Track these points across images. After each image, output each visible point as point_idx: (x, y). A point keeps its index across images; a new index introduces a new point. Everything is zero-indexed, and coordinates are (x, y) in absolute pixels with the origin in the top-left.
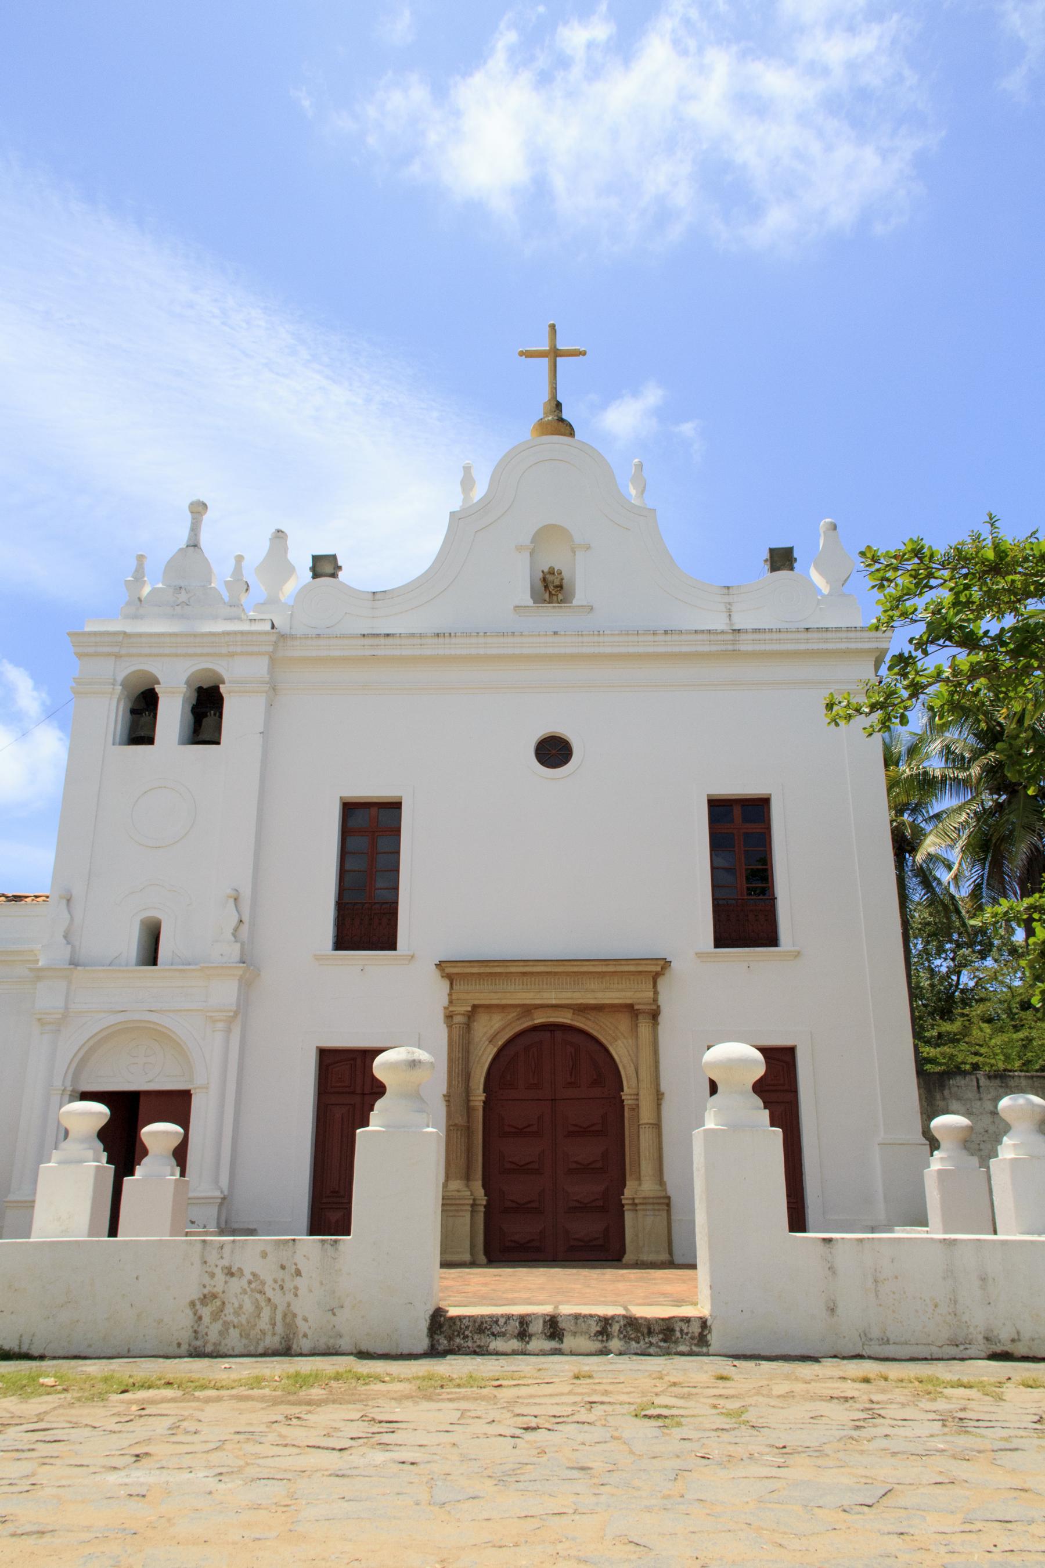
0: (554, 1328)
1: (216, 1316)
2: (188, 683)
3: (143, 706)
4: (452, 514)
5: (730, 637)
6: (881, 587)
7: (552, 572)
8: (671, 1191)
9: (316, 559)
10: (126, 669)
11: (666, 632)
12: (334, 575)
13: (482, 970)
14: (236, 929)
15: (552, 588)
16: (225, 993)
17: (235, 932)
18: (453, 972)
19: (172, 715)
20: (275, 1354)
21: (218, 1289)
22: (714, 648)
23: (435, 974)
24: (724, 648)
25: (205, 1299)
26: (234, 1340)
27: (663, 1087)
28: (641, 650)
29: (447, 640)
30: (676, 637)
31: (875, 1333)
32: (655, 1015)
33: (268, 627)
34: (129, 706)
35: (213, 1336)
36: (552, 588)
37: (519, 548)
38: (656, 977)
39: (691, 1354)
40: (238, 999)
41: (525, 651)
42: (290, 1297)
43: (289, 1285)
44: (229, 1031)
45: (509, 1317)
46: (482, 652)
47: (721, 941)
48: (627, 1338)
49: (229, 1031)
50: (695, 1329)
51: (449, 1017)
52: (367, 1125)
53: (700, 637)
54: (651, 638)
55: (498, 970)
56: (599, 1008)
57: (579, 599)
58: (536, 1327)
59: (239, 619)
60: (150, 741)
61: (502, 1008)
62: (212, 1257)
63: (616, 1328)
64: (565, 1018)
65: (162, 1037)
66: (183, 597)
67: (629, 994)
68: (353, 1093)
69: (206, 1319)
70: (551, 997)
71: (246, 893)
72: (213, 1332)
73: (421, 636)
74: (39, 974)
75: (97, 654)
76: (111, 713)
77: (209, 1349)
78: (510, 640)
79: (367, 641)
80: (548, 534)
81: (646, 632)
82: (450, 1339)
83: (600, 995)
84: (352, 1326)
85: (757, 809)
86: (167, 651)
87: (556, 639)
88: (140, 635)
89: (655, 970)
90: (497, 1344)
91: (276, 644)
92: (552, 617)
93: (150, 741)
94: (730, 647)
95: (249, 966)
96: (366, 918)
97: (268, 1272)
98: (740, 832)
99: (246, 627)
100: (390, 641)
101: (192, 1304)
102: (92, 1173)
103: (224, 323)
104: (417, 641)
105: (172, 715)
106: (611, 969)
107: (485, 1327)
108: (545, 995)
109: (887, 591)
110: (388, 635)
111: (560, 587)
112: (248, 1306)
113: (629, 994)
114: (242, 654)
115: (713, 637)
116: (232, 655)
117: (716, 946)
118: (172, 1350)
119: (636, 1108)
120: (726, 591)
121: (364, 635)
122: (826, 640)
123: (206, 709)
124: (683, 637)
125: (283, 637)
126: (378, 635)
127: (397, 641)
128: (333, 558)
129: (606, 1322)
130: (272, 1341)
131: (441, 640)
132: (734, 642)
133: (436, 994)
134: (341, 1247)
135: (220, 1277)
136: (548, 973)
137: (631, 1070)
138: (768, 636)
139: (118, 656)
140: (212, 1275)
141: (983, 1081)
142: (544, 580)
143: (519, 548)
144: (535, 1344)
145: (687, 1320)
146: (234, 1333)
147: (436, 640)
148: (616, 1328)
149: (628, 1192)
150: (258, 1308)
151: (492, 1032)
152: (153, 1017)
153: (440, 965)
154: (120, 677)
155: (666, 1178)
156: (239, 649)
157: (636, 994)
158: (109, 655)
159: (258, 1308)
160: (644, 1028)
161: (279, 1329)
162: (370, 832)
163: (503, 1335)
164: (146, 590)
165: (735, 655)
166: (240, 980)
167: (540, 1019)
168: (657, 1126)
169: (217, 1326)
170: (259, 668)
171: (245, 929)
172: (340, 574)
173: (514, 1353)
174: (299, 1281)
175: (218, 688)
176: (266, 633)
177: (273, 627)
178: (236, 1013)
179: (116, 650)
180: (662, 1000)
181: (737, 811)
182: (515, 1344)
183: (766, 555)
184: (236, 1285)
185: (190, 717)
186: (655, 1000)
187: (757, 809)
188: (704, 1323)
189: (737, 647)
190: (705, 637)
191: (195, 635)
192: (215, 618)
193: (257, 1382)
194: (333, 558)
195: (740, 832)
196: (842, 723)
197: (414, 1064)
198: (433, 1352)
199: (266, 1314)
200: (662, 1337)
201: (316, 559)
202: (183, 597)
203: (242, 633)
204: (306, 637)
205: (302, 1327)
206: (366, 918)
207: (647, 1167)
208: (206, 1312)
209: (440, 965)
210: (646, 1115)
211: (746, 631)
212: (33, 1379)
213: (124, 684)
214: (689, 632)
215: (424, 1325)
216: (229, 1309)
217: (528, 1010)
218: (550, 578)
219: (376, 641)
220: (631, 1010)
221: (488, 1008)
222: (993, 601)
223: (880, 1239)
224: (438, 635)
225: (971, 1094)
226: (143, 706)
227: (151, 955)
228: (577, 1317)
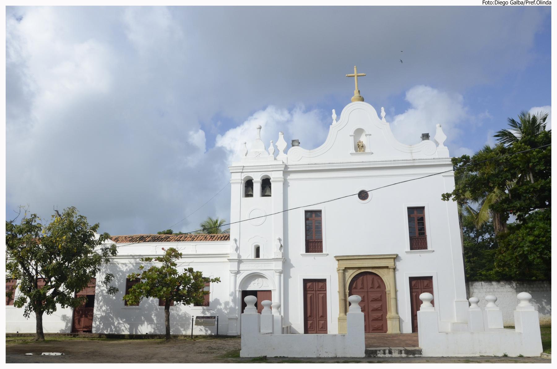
3: (249, 184)
10: (244, 176)
16: (279, 266)
18: (339, 259)
19: (257, 188)
33: (282, 163)
44: (280, 276)
49: (280, 276)
60: (251, 196)
71: (282, 238)
85: (318, 213)
89: (396, 258)
93: (251, 196)
96: (313, 244)
98: (416, 217)
105: (257, 188)
119: (389, 294)
123: (266, 184)
153: (335, 257)
157: (390, 263)
162: (313, 219)
170: (280, 175)
179: (241, 171)
183: (421, 135)
187: (318, 213)
195: (416, 217)
206: (313, 244)
210: (392, 295)
217: (360, 268)
218: (359, 144)
225: (479, 287)
227: (258, 255)
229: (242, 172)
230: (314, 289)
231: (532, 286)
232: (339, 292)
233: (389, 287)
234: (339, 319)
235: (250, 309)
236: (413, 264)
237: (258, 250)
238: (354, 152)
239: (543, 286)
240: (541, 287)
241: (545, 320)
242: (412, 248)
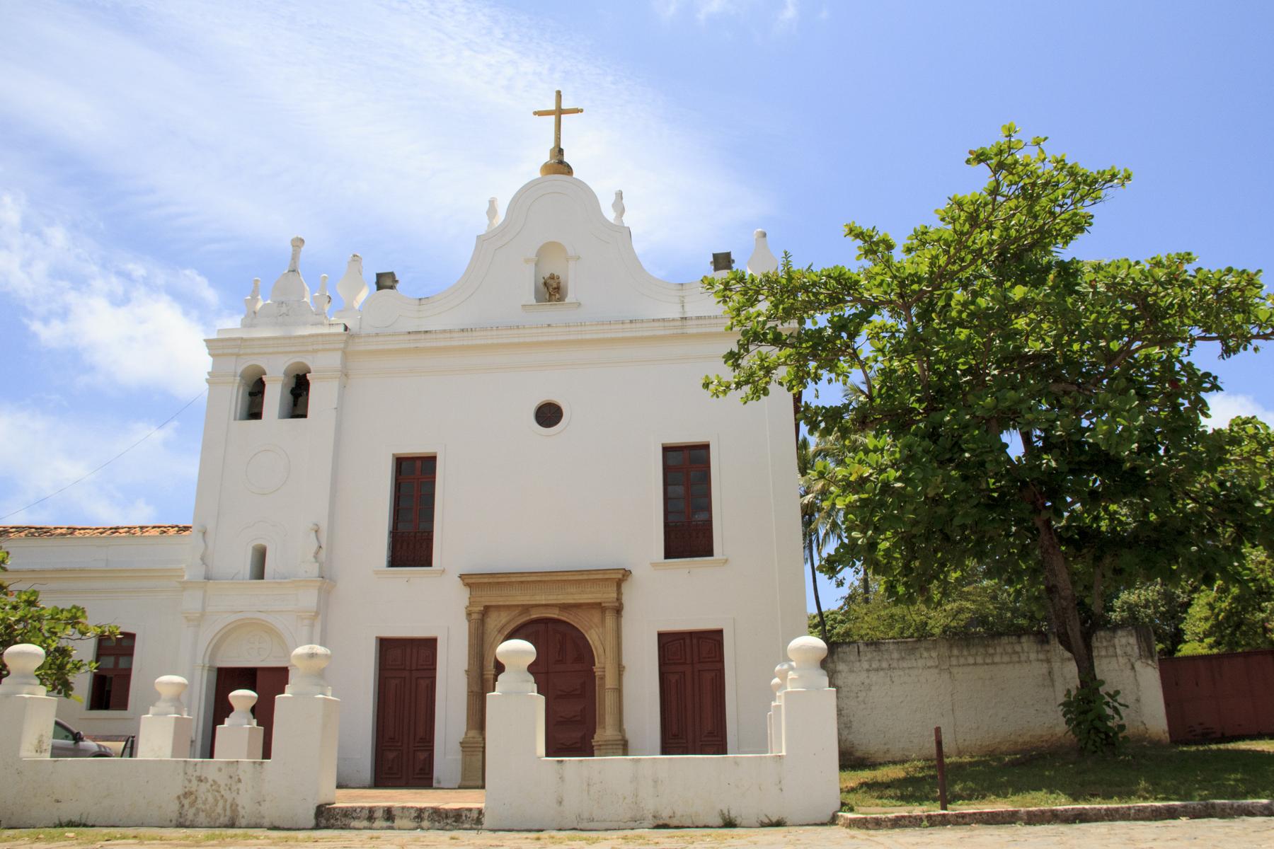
0: (389, 814)
1: (192, 804)
2: (286, 374)
3: (256, 391)
4: (478, 237)
5: (679, 323)
6: (725, 302)
7: (552, 277)
8: (629, 735)
9: (379, 276)
11: (631, 322)
12: (391, 287)
14: (317, 553)
15: (552, 290)
16: (309, 599)
17: (316, 555)
18: (472, 581)
19: (274, 397)
20: (226, 826)
21: (193, 789)
22: (668, 332)
25: (186, 795)
26: (202, 818)
27: (624, 662)
28: (613, 335)
30: (638, 325)
31: (586, 815)
32: (618, 611)
33: (341, 329)
34: (248, 390)
35: (190, 816)
36: (552, 290)
37: (527, 261)
38: (619, 584)
39: (471, 829)
40: (319, 602)
41: (528, 340)
42: (234, 794)
43: (234, 788)
44: (312, 626)
45: (363, 808)
46: (495, 341)
48: (433, 820)
50: (475, 815)
51: (469, 614)
53: (656, 324)
57: (570, 298)
58: (379, 814)
59: (322, 324)
61: (508, 607)
62: (190, 770)
63: (426, 814)
64: (554, 614)
65: (270, 630)
66: (284, 309)
68: (685, 663)
69: (187, 806)
70: (541, 599)
71: (324, 525)
72: (190, 813)
73: (451, 331)
74: (185, 586)
75: (224, 355)
76: (234, 396)
77: (188, 823)
78: (516, 331)
79: (412, 337)
80: (549, 249)
81: (617, 322)
82: (328, 820)
83: (577, 597)
84: (270, 812)
86: (271, 350)
87: (550, 330)
88: (252, 339)
89: (620, 578)
90: (355, 823)
91: (346, 342)
92: (552, 313)
94: (679, 331)
95: (326, 580)
96: (411, 544)
97: (222, 780)
98: (687, 470)
99: (326, 330)
100: (428, 336)
101: (179, 797)
102: (173, 722)
103: (431, 13)
104: (448, 335)
105: (274, 397)
106: (585, 577)
107: (348, 814)
108: (538, 598)
109: (730, 304)
111: (558, 289)
112: (211, 800)
114: (324, 350)
116: (316, 351)
117: (667, 557)
118: (168, 823)
119: (603, 678)
123: (299, 388)
124: (645, 325)
125: (352, 336)
127: (434, 336)
128: (392, 275)
129: (420, 811)
130: (223, 820)
132: (683, 327)
133: (459, 598)
134: (265, 766)
135: (195, 782)
137: (601, 651)
138: (707, 322)
139: (238, 355)
140: (190, 781)
142: (545, 284)
143: (527, 261)
144: (377, 824)
145: (470, 810)
146: (202, 815)
147: (461, 334)
148: (426, 814)
149: (596, 737)
150: (216, 801)
151: (500, 625)
152: (262, 616)
153: (461, 576)
154: (239, 372)
155: (625, 726)
156: (320, 347)
157: (608, 595)
158: (232, 354)
159: (216, 801)
160: (610, 620)
161: (228, 813)
162: (414, 480)
163: (359, 818)
164: (260, 304)
165: (684, 336)
166: (320, 589)
168: (619, 691)
169: (193, 810)
171: (323, 553)
172: (398, 286)
173: (365, 828)
174: (240, 786)
175: (305, 376)
176: (339, 334)
177: (346, 328)
178: (317, 614)
179: (236, 351)
180: (625, 599)
182: (366, 823)
184: (204, 787)
185: (289, 397)
186: (619, 599)
188: (480, 812)
190: (661, 324)
191: (290, 338)
192: (305, 324)
193: (187, 837)
194: (392, 275)
195: (687, 470)
196: (721, 395)
197: (312, 656)
198: (317, 827)
199: (221, 803)
200: (455, 820)
201: (379, 276)
202: (284, 309)
203: (322, 335)
204: (369, 336)
205: (242, 812)
206: (411, 544)
207: (609, 719)
208: (186, 802)
209: (461, 576)
210: (610, 682)
211: (691, 318)
212: (63, 834)
213: (242, 376)
214: (648, 321)
215: (312, 812)
216: (199, 801)
217: (526, 608)
219: (418, 337)
220: (598, 606)
221: (498, 608)
222: (788, 314)
226: (256, 391)
227: (259, 572)
228: (403, 808)
229: (238, 355)
230: (404, 669)
231: (991, 651)
232: (467, 672)
233: (603, 662)
234: (463, 745)
235: (238, 730)
236: (669, 598)
237: (260, 556)
238: (534, 302)
239: (1018, 648)
240: (1015, 652)
241: (1021, 740)
242: (669, 554)
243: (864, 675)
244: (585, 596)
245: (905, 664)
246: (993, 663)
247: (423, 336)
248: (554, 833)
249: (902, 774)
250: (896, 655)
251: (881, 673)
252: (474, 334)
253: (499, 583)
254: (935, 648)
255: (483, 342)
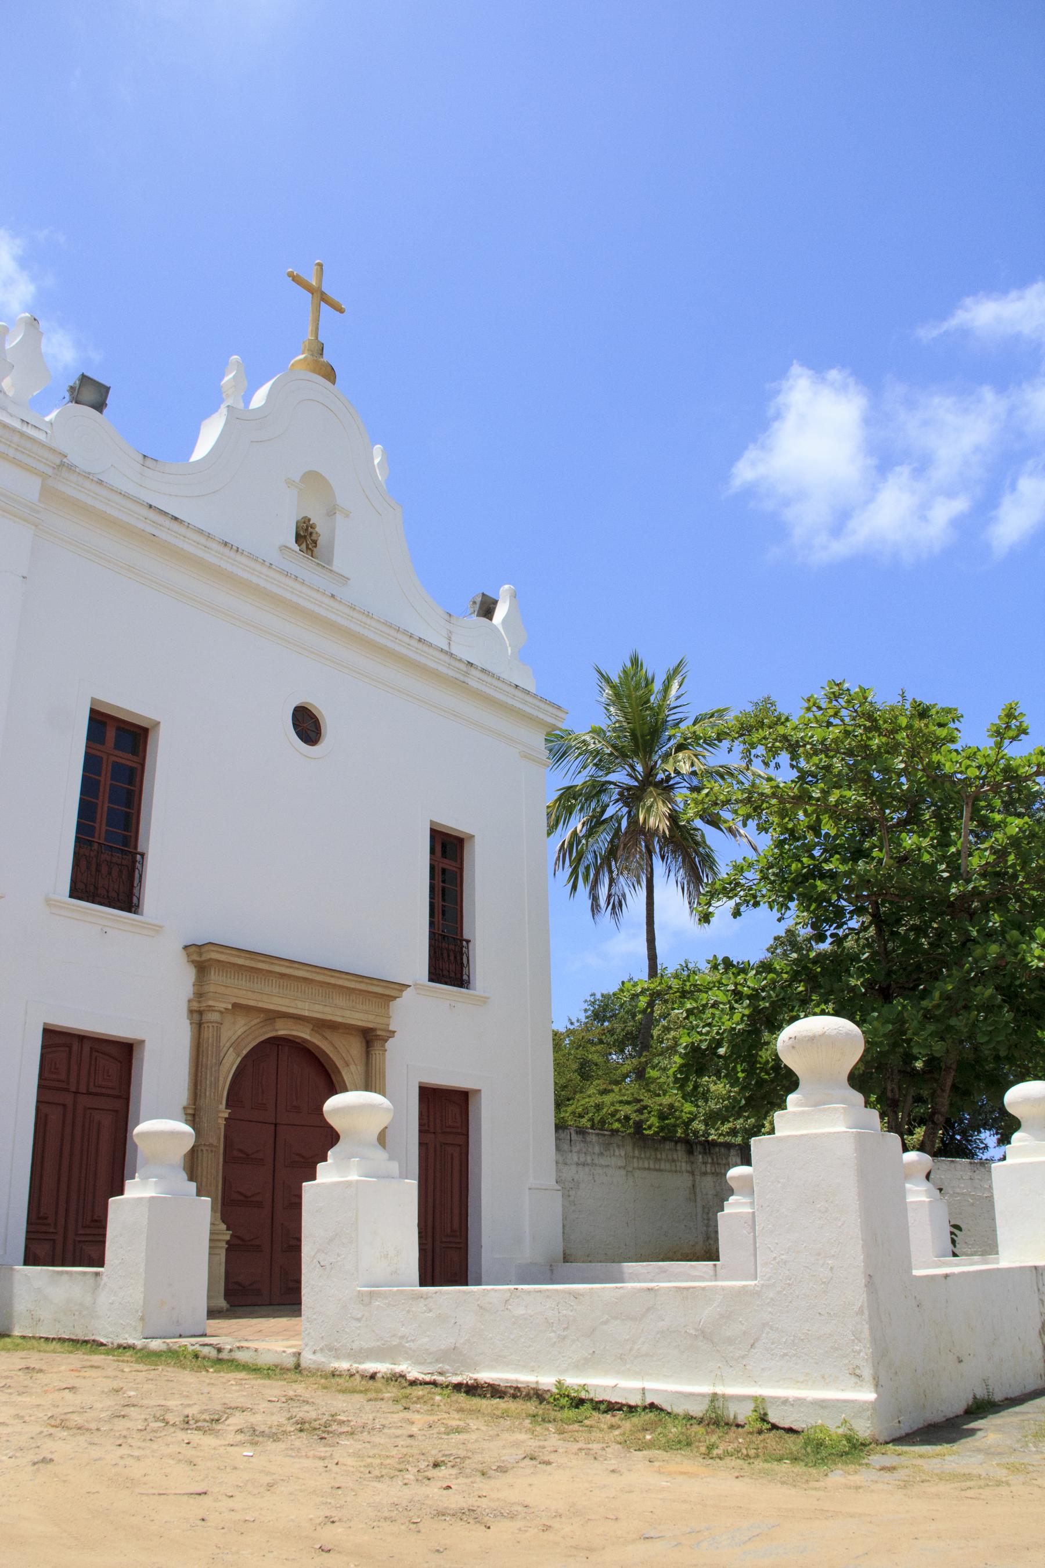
5: (463, 667)
11: (420, 640)
13: (248, 963)
18: (205, 959)
22: (451, 673)
23: (181, 958)
24: (457, 676)
29: (232, 554)
30: (425, 648)
47: (76, 892)
52: (314, 1178)
54: (407, 639)
55: (260, 965)
56: (333, 1026)
64: (304, 1033)
67: (371, 1018)
68: (67, 1090)
73: (209, 536)
79: (152, 515)
83: (347, 1013)
87: (332, 603)
94: (462, 678)
96: (108, 865)
100: (175, 526)
104: (203, 540)
106: (363, 987)
108: (300, 1004)
110: (176, 519)
113: (371, 1018)
115: (453, 662)
120: (447, 617)
121: (151, 506)
122: (526, 702)
124: (431, 651)
126: (166, 514)
127: (182, 530)
131: (226, 551)
133: (181, 981)
136: (305, 980)
141: (574, 1136)
147: (221, 548)
157: (358, 1016)
165: (460, 686)
167: (283, 1029)
181: (126, 759)
189: (466, 680)
206: (108, 865)
217: (273, 1016)
223: (557, 1290)
224: (226, 544)
240: (674, 1161)
243: (574, 1168)
244: (357, 1015)
245: (603, 1161)
246: (660, 1170)
247: (168, 523)
248: (440, 1379)
249: (164, 1347)
250: (597, 1149)
251: (587, 1169)
252: (239, 558)
253: (252, 969)
254: (623, 1146)
255: (246, 575)
